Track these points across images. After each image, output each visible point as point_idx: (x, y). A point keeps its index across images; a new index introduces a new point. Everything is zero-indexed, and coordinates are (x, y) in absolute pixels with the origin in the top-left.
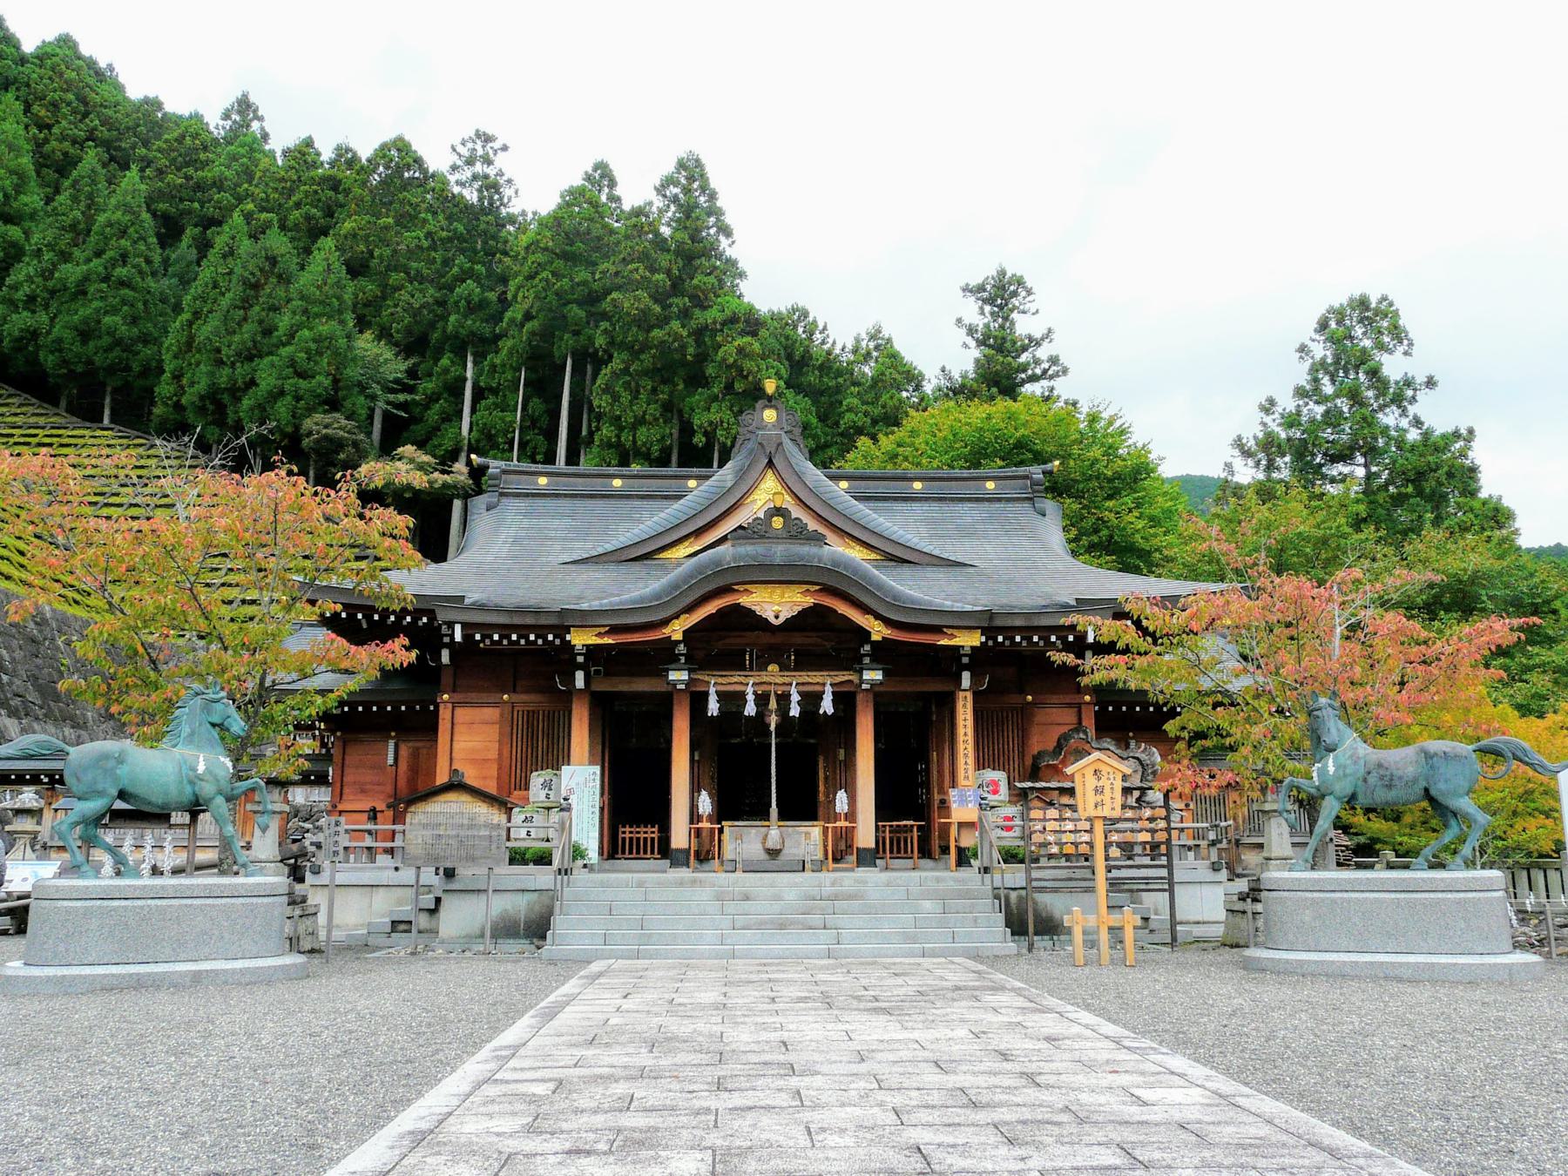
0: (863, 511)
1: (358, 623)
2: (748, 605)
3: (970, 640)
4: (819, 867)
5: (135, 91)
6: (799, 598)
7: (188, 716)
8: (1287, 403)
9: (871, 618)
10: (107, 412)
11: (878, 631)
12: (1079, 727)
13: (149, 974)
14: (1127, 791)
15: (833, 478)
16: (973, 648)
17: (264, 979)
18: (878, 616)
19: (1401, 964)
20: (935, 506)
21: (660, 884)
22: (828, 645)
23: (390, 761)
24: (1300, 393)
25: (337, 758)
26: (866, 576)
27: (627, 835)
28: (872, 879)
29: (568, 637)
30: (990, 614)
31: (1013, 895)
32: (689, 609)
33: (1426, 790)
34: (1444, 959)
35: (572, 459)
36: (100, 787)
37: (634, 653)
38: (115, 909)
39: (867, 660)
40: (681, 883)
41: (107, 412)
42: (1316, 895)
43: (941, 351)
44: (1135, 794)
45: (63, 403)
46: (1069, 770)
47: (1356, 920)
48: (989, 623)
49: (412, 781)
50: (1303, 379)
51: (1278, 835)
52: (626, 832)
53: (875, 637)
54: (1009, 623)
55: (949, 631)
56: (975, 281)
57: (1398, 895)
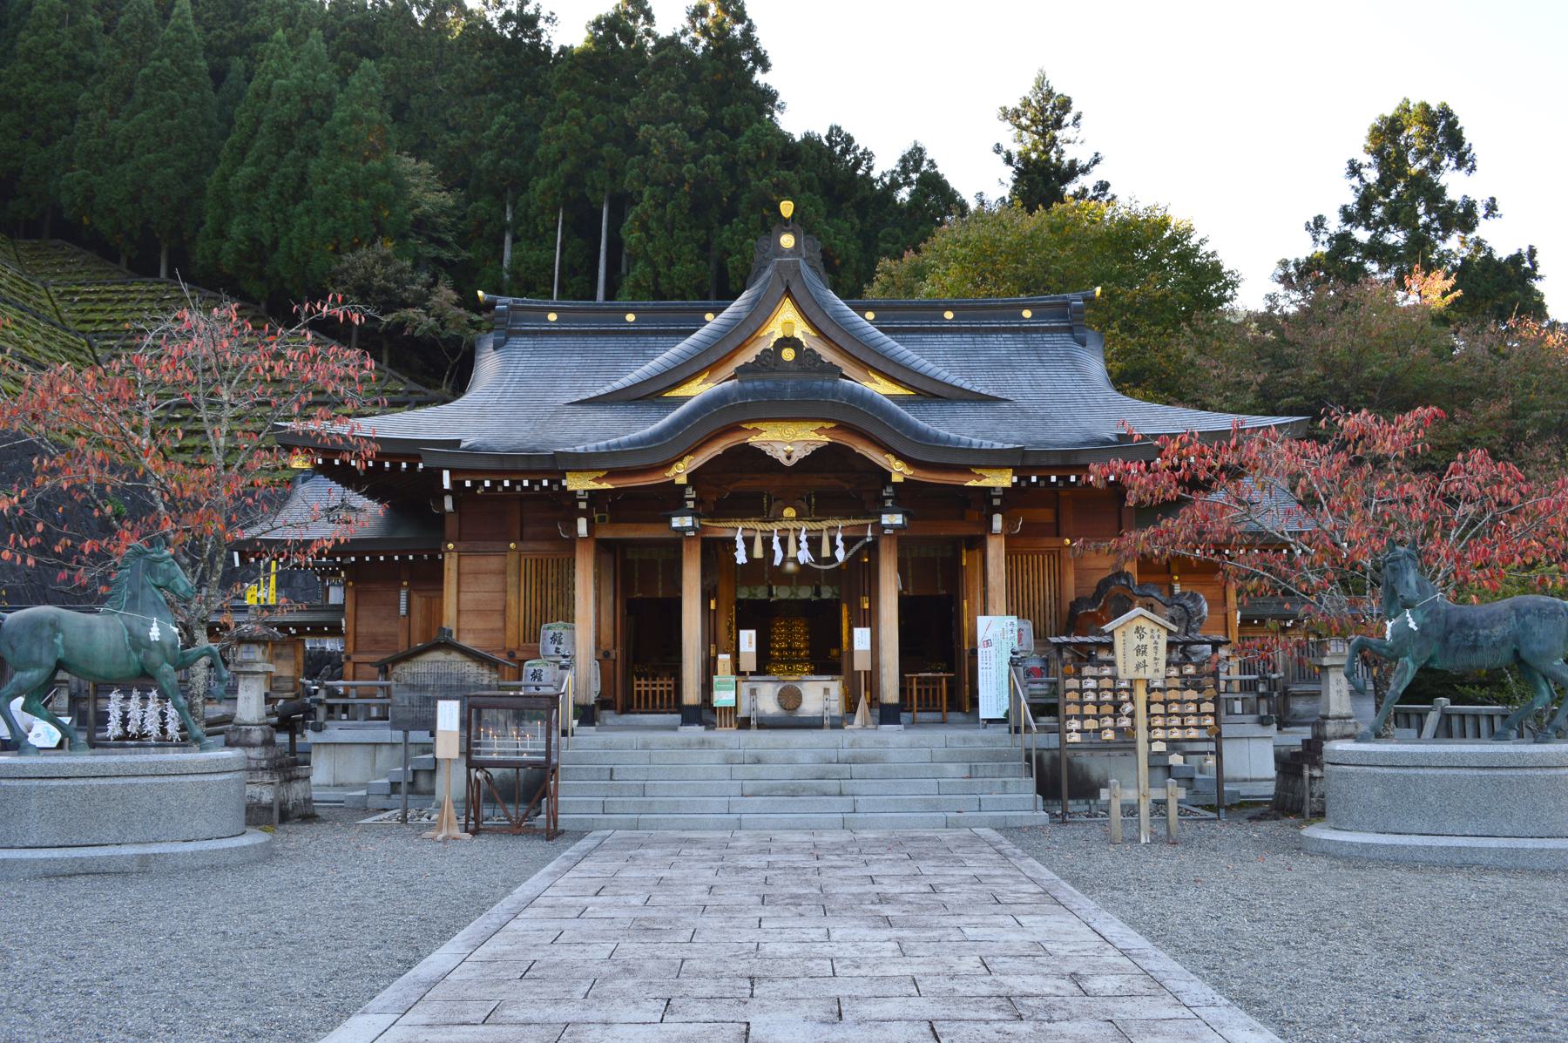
0: (890, 343)
2: (757, 445)
3: (1003, 480)
6: (813, 436)
8: (1334, 225)
9: (891, 458)
11: (899, 471)
13: (93, 859)
14: (1171, 646)
15: (861, 310)
16: (1005, 489)
17: (215, 866)
19: (1481, 850)
20: (967, 338)
21: (669, 746)
22: (847, 487)
23: (403, 611)
24: (1347, 216)
25: (349, 608)
27: (643, 689)
29: (564, 483)
30: (1021, 452)
31: (1047, 756)
32: (693, 451)
33: (1516, 652)
34: (1529, 844)
35: (609, 296)
36: (36, 656)
37: (635, 500)
38: (54, 789)
39: (889, 503)
40: (688, 745)
42: (1386, 770)
44: (1179, 650)
45: (123, 261)
46: (1107, 627)
47: (1431, 799)
48: (1017, 460)
49: (426, 633)
50: (1351, 199)
51: (1337, 695)
52: (641, 685)
53: (896, 478)
54: (1044, 461)
55: (978, 472)
56: (1014, 103)
57: (1481, 772)
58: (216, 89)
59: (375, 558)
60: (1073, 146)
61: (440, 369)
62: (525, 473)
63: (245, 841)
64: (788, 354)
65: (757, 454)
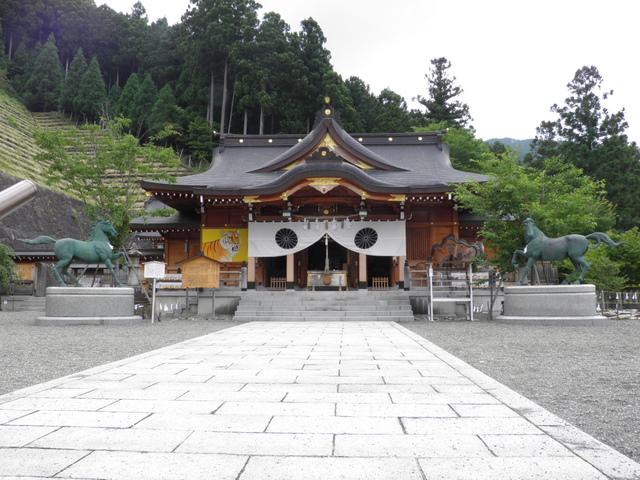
1: (163, 194)
4: (344, 289)
5: (118, 12)
6: (333, 183)
7: (98, 228)
10: (327, 261)
11: (364, 195)
12: (452, 235)
18: (364, 190)
25: (166, 251)
26: (364, 178)
28: (363, 292)
30: (408, 188)
32: (290, 188)
41: (327, 261)
43: (414, 95)
48: (407, 191)
53: (363, 198)
58: (141, 82)
59: (183, 195)
60: (447, 74)
61: (197, 152)
62: (230, 196)
63: (131, 318)
64: (324, 153)
65: (313, 190)
